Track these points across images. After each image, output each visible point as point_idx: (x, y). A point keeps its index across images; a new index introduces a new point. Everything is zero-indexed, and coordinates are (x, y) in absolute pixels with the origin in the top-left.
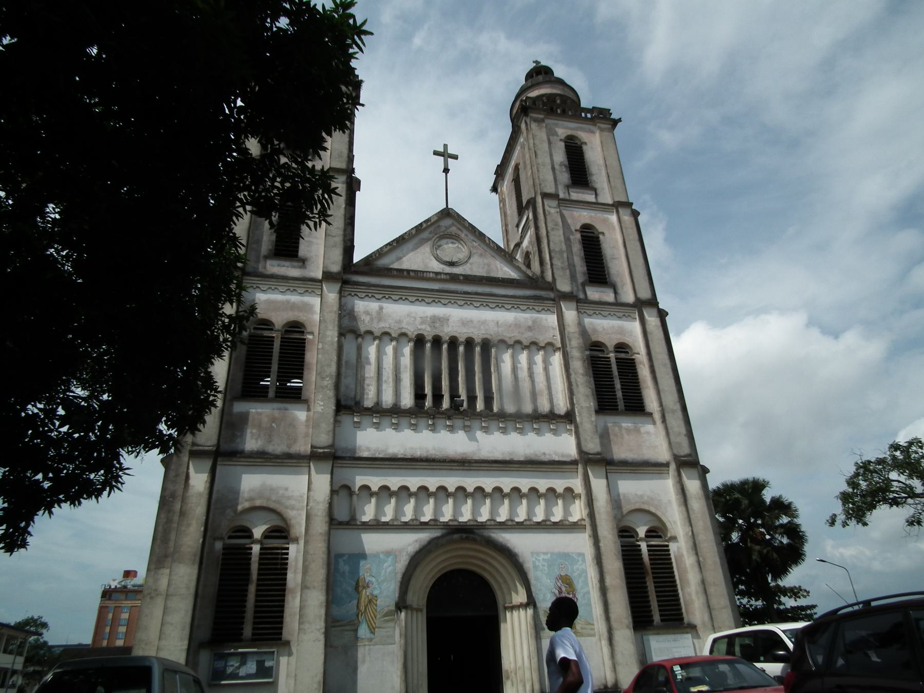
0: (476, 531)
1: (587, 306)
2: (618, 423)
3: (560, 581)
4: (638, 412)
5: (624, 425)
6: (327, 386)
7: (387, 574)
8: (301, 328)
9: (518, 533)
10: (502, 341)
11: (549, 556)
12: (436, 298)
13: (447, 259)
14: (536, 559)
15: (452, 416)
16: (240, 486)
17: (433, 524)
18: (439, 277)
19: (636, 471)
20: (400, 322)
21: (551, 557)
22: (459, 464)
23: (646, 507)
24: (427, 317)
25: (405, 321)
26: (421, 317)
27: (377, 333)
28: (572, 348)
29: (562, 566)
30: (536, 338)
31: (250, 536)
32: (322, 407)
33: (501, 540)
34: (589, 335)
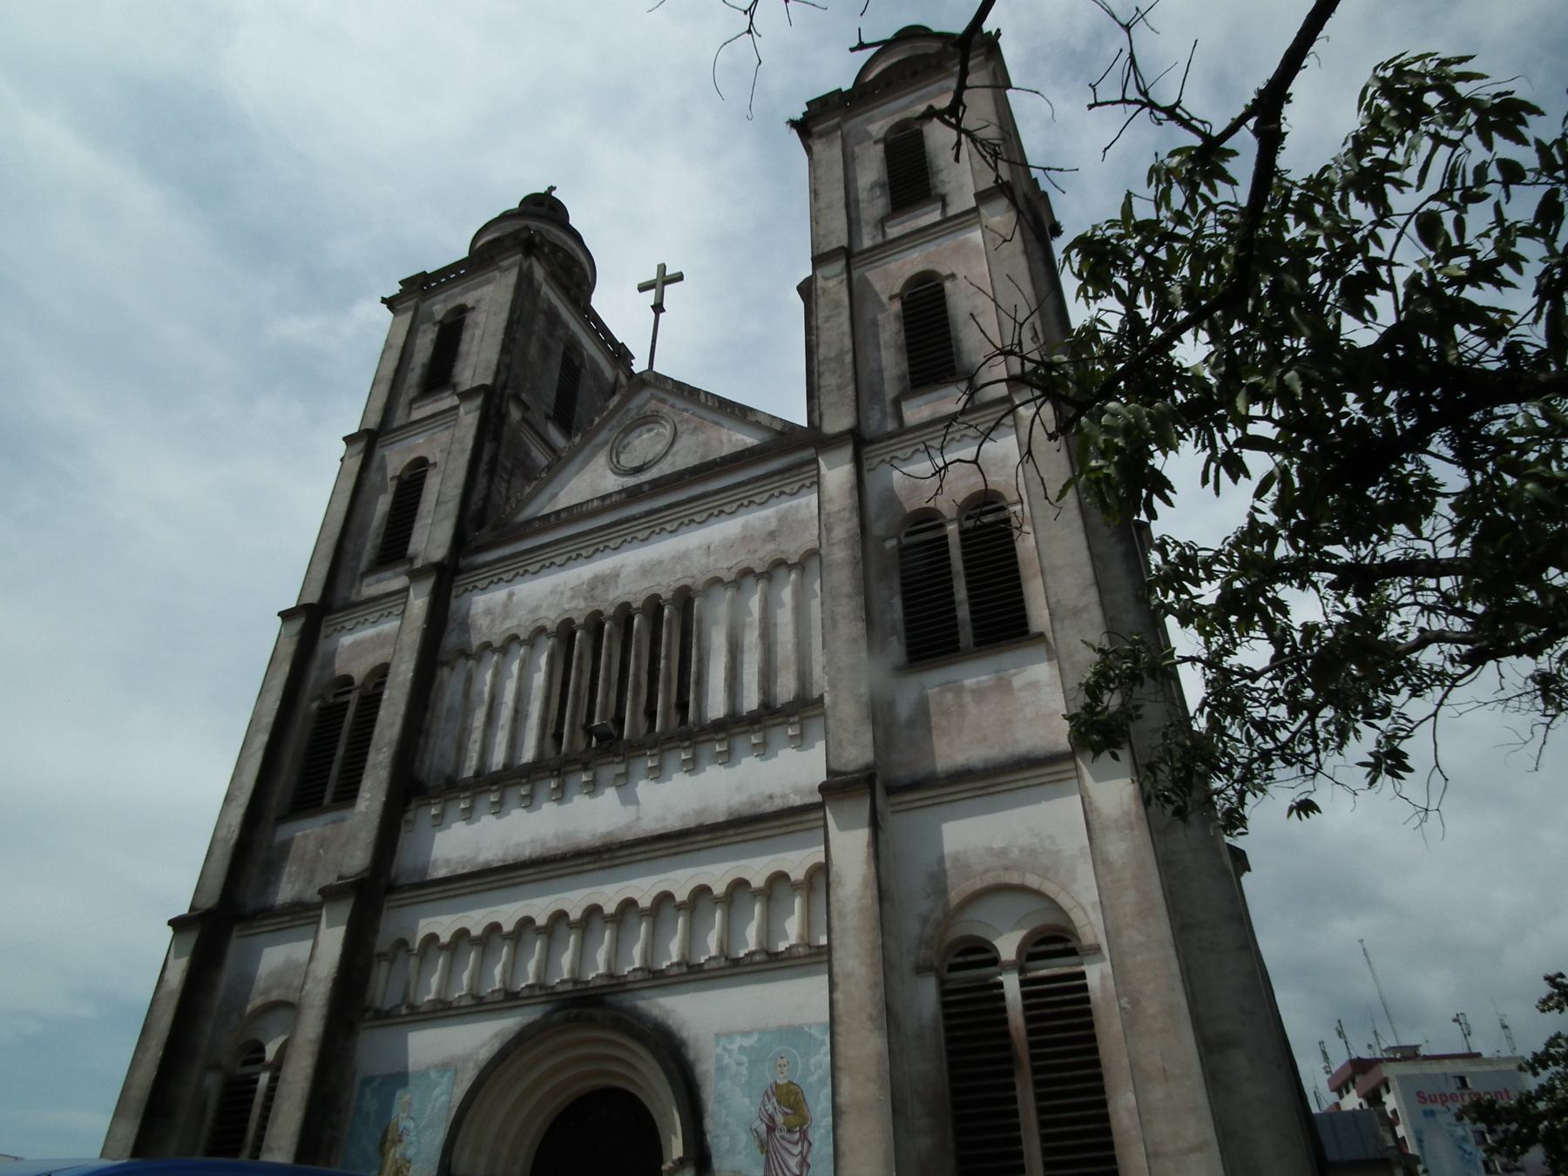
0: (609, 999)
1: (896, 444)
2: (955, 681)
3: (774, 1100)
4: (1003, 642)
5: (969, 682)
6: (381, 763)
7: (436, 1110)
8: (996, 503)
9: (695, 991)
10: (716, 581)
11: (755, 1037)
12: (626, 534)
13: (636, 464)
14: (725, 1049)
15: (590, 762)
16: (256, 971)
17: (541, 990)
18: (608, 502)
19: (991, 790)
20: (538, 607)
21: (760, 1039)
22: (592, 858)
23: (1014, 878)
24: (583, 583)
25: (545, 604)
26: (572, 588)
27: (727, 577)
28: (833, 545)
29: (784, 1061)
30: (782, 552)
31: (995, 961)
32: (367, 803)
33: (655, 1012)
34: (901, 503)
